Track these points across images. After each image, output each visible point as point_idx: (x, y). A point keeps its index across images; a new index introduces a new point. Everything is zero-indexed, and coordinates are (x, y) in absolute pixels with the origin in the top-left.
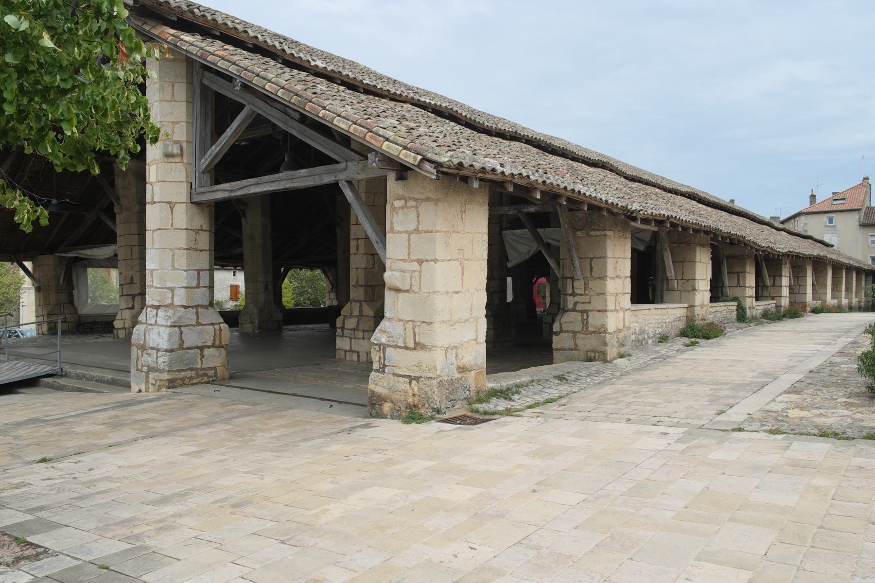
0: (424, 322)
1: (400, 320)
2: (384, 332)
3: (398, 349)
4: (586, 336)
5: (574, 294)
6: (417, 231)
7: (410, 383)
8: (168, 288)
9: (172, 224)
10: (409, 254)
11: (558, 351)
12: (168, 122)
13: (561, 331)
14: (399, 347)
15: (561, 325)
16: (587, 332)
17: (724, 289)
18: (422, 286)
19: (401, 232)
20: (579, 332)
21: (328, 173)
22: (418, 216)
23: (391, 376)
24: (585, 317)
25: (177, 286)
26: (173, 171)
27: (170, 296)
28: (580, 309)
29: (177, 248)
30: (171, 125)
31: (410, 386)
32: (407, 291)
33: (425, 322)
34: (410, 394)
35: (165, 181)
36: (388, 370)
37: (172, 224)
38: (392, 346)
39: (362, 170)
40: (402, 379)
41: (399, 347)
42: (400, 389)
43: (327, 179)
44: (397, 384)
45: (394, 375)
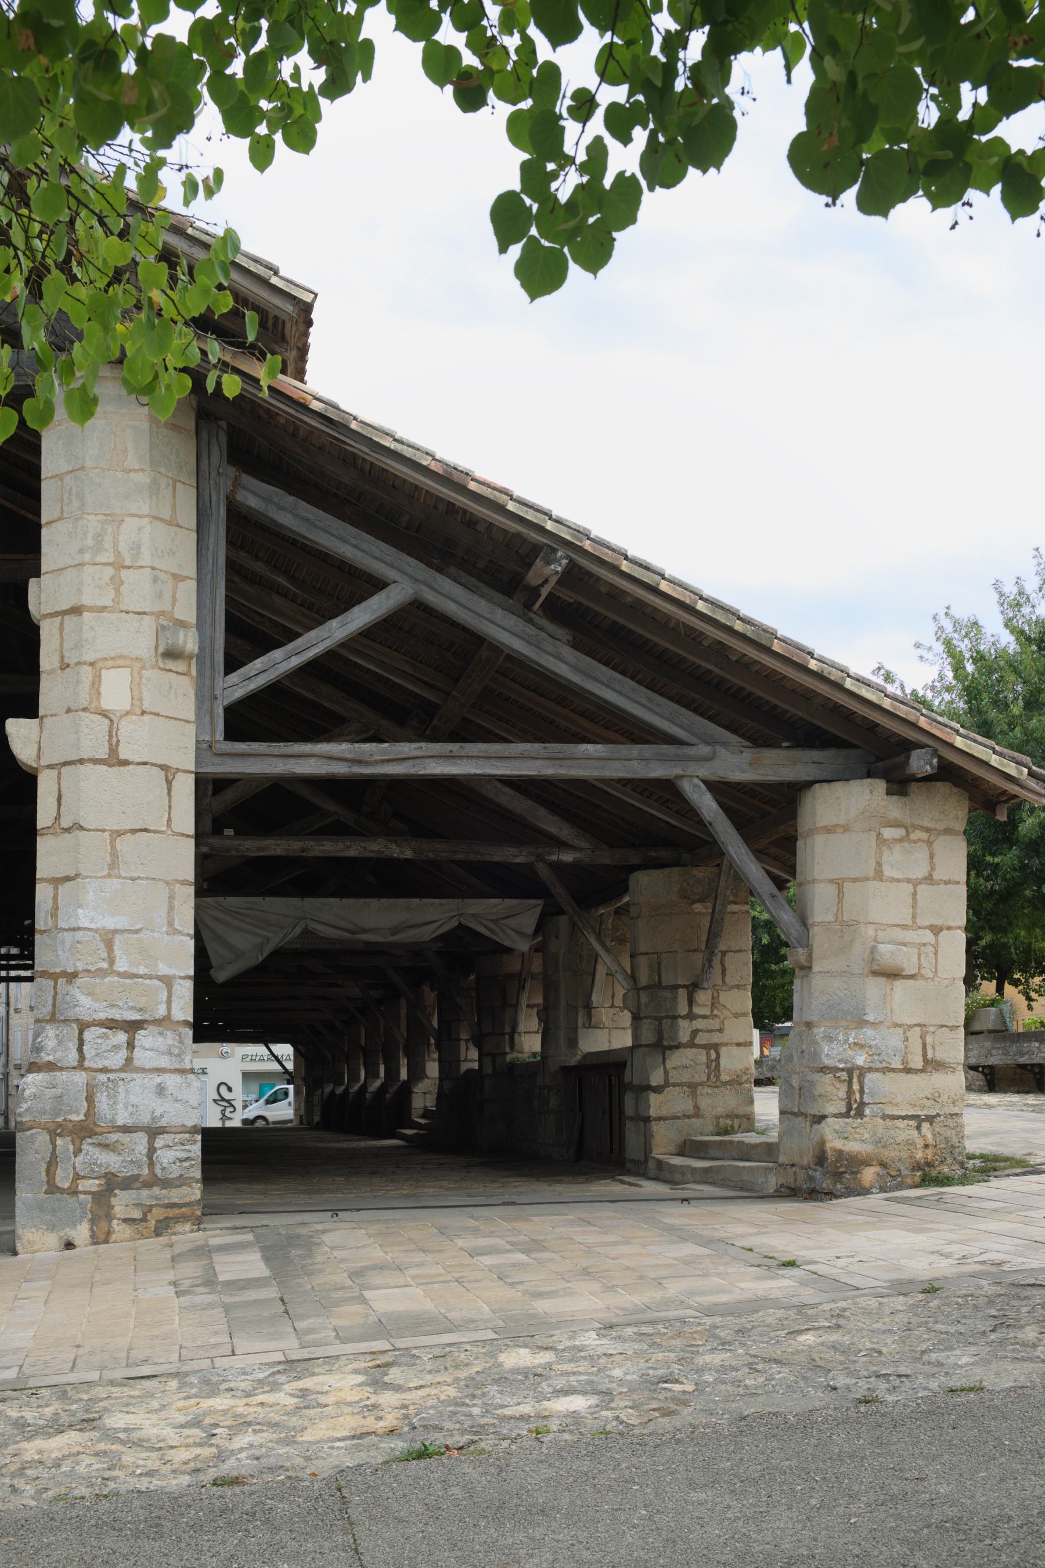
0: (943, 1026)
1: (896, 1025)
2: (862, 1046)
3: (891, 1074)
4: (716, 1090)
5: (691, 1016)
6: (929, 879)
7: (918, 1128)
8: (160, 978)
9: (169, 820)
10: (914, 917)
11: (662, 1122)
12: (166, 572)
13: (667, 1084)
14: (893, 1070)
15: (666, 1072)
16: (718, 1084)
17: (516, 1036)
18: (939, 967)
19: (898, 881)
20: (701, 1084)
21: (662, 759)
22: (932, 857)
23: (879, 1120)
24: (713, 1056)
25: (178, 973)
26: (173, 691)
27: (165, 998)
28: (704, 1042)
29: (177, 881)
30: (170, 582)
31: (920, 1133)
32: (912, 977)
33: (946, 1026)
34: (920, 1143)
35: (158, 715)
36: (872, 1110)
37: (169, 820)
38: (877, 1070)
39: (750, 765)
40: (901, 1124)
41: (893, 1070)
42: (899, 1140)
43: (658, 771)
44: (892, 1132)
45: (884, 1117)
